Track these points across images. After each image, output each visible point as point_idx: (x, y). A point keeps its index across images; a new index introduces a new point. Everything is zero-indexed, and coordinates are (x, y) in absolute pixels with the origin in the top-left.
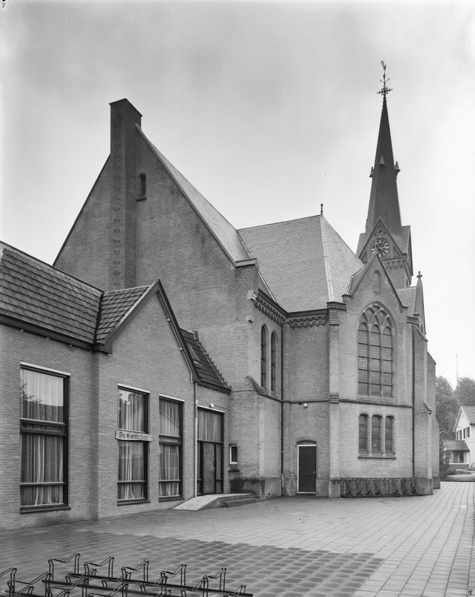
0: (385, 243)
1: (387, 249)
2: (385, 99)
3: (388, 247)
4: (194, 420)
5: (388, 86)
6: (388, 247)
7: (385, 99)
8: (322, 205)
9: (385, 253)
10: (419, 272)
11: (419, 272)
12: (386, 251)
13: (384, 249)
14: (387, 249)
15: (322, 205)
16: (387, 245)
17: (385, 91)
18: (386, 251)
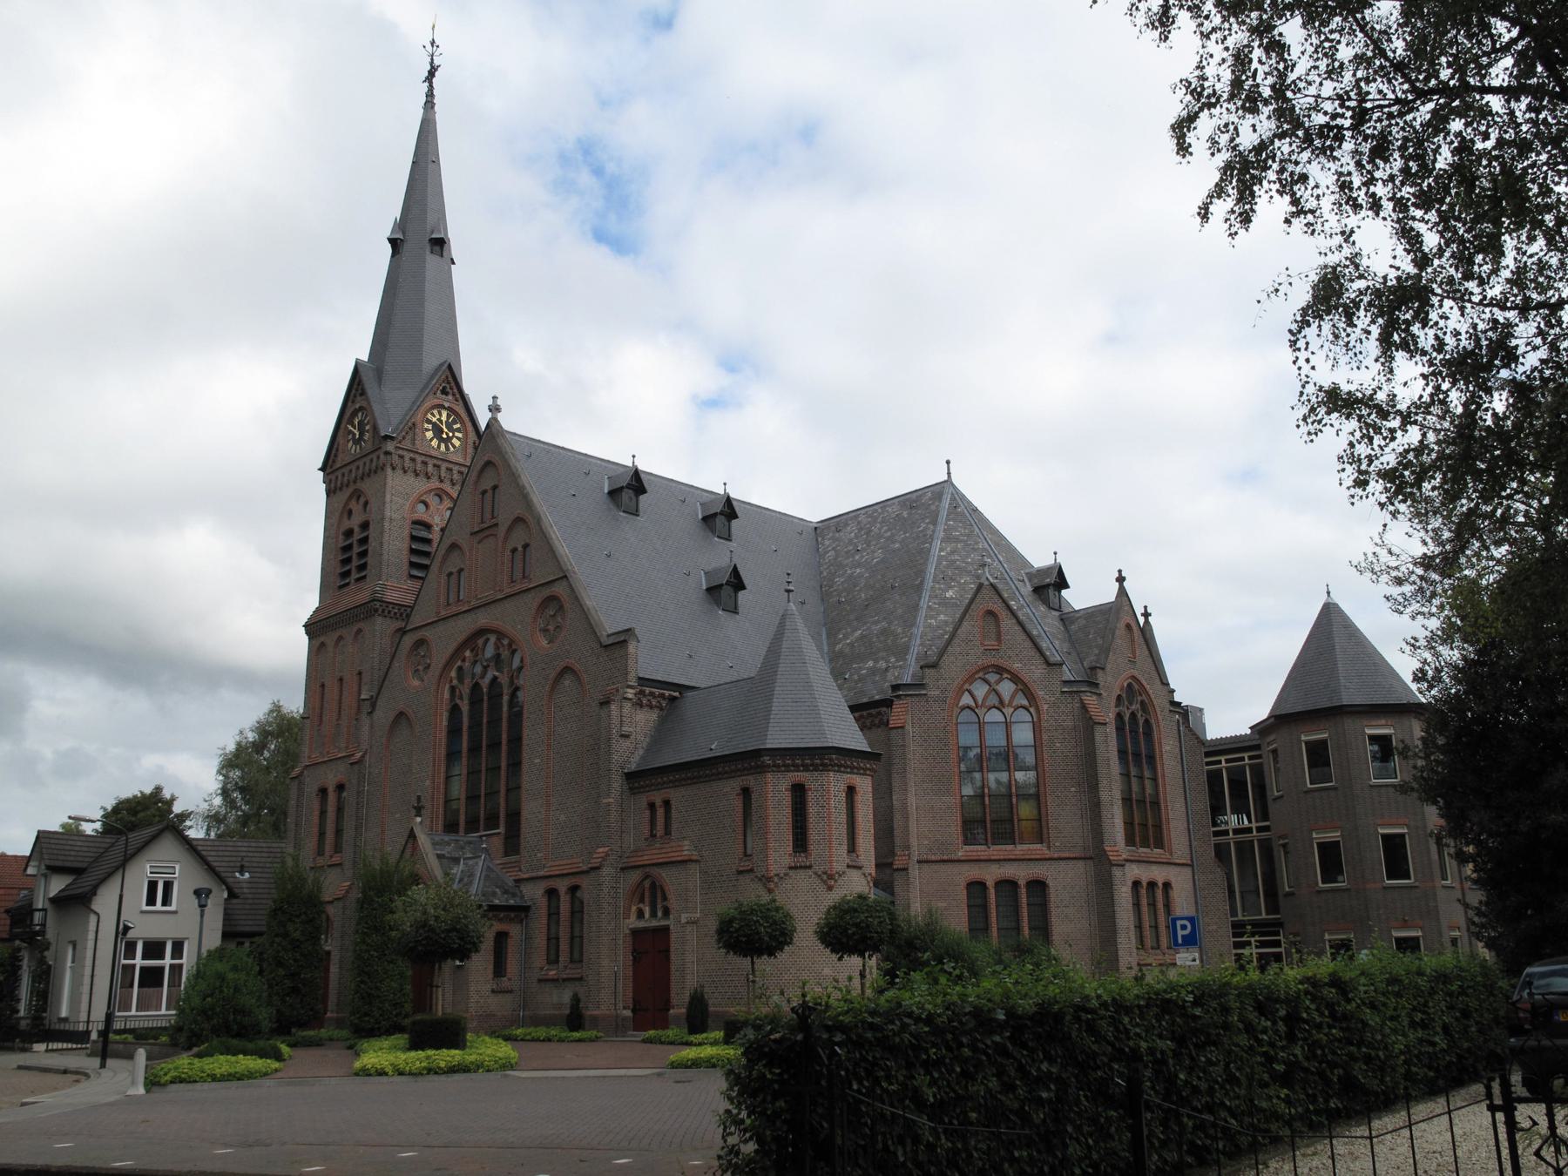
8: (948, 462)
15: (948, 462)
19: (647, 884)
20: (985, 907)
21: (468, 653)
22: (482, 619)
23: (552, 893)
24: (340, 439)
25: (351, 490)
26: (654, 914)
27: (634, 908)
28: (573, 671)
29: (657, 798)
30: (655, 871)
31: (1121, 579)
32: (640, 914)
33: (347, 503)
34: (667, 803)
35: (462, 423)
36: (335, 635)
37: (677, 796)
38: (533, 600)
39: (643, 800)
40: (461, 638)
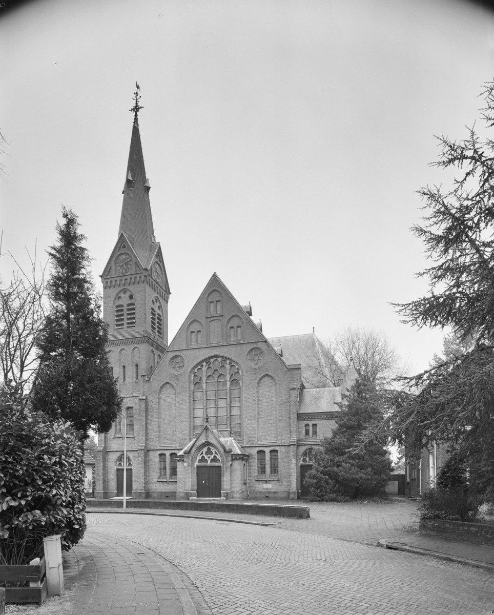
2: (136, 115)
5: (140, 104)
7: (136, 115)
17: (136, 109)
21: (204, 364)
22: (215, 352)
29: (311, 423)
34: (314, 425)
36: (133, 347)
39: (303, 424)
40: (203, 358)
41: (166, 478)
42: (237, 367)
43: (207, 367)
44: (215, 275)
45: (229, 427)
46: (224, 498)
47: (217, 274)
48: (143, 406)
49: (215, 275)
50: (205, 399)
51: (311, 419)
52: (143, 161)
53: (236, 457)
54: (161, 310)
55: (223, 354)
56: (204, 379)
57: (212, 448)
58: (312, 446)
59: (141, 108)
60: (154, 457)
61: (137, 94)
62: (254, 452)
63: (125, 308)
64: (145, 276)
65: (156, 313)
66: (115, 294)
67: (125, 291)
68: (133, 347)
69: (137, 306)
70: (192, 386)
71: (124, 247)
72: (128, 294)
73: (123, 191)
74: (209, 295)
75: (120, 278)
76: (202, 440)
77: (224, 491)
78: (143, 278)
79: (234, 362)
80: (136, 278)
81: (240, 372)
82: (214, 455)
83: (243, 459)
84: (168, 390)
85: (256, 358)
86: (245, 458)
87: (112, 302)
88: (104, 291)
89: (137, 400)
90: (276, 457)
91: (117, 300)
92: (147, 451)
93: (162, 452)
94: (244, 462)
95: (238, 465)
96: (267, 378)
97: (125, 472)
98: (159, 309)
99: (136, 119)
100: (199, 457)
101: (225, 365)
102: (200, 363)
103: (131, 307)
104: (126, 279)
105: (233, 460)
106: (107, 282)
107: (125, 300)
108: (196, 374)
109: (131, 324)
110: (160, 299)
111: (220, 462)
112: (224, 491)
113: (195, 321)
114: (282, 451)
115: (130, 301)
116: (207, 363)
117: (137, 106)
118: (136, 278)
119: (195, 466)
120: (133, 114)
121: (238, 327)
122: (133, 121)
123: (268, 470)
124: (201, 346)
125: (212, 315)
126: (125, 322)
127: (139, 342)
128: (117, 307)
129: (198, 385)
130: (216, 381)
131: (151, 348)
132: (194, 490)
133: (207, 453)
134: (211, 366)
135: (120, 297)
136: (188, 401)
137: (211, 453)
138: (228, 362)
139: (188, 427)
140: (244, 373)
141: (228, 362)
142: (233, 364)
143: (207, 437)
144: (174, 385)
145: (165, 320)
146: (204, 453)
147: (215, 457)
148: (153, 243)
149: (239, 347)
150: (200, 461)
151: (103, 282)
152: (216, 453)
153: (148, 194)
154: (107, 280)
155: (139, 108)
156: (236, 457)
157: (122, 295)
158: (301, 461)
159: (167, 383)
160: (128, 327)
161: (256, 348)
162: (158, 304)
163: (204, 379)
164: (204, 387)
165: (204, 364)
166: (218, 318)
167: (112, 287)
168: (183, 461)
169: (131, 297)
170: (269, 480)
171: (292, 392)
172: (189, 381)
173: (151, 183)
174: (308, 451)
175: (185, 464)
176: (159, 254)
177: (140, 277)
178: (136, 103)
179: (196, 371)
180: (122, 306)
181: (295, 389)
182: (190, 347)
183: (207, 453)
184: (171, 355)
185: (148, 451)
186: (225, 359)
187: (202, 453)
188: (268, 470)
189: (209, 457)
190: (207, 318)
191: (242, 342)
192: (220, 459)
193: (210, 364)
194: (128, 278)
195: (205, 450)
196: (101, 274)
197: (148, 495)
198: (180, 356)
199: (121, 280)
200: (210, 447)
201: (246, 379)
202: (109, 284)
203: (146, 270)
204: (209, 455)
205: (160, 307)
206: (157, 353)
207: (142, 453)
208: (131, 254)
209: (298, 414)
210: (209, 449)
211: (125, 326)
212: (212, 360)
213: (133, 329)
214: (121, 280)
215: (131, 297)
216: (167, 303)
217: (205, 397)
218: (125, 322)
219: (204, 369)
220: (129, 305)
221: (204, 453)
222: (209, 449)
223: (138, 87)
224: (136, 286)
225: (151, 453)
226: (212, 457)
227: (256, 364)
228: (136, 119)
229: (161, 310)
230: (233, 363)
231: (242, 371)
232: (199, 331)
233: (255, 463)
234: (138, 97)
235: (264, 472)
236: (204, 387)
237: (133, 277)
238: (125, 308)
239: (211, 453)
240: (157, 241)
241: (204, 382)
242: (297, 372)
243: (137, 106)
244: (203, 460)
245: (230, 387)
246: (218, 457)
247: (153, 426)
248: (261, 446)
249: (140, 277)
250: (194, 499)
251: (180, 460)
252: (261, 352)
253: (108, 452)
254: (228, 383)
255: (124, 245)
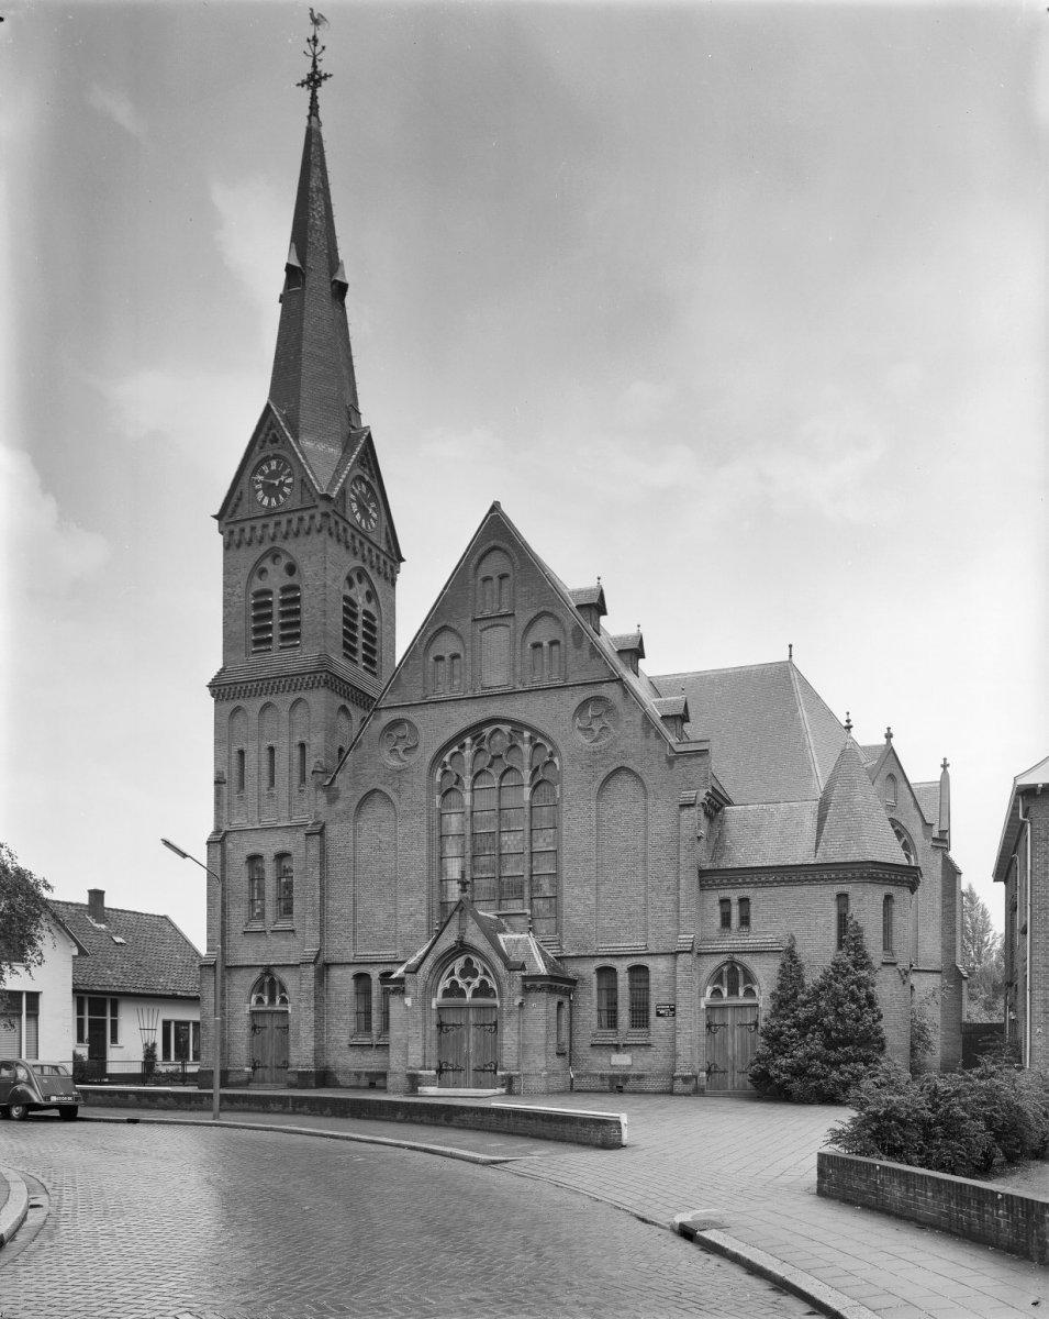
0: (285, 468)
1: (289, 485)
2: (314, 98)
3: (290, 480)
4: (559, 1018)
5: (323, 68)
6: (290, 480)
7: (314, 98)
8: (790, 646)
9: (284, 495)
10: (945, 759)
11: (945, 759)
12: (286, 490)
13: (282, 484)
14: (289, 485)
15: (790, 646)
16: (289, 475)
17: (314, 80)
18: (286, 490)
19: (267, 980)
20: (368, 1013)
21: (468, 741)
22: (495, 709)
23: (606, 973)
24: (244, 485)
25: (264, 548)
26: (272, 1000)
27: (254, 997)
28: (629, 771)
29: (734, 895)
30: (276, 970)
31: (945, 766)
32: (260, 1000)
33: (258, 563)
34: (744, 901)
35: (378, 505)
36: (292, 697)
37: (756, 895)
38: (574, 699)
39: (714, 898)
40: (463, 725)
41: (370, 1036)
42: (549, 749)
43: (475, 748)
44: (495, 507)
45: (527, 903)
46: (504, 1090)
47: (505, 508)
48: (314, 851)
49: (495, 507)
50: (468, 833)
51: (734, 885)
52: (332, 216)
53: (531, 984)
54: (373, 603)
55: (514, 716)
56: (467, 779)
57: (475, 959)
58: (736, 957)
59: (326, 76)
60: (342, 980)
61: (315, 40)
62: (588, 970)
63: (276, 598)
64: (325, 515)
65: (360, 610)
66: (250, 564)
67: (275, 555)
68: (292, 697)
69: (305, 594)
70: (438, 797)
71: (275, 440)
72: (284, 561)
73: (281, 296)
74: (483, 557)
75: (263, 521)
76: (448, 940)
77: (503, 1073)
78: (318, 518)
79: (542, 736)
80: (301, 519)
81: (556, 760)
82: (480, 977)
83: (552, 990)
84: (377, 810)
85: (596, 726)
86: (559, 984)
87: (243, 584)
88: (225, 555)
89: (300, 836)
90: (643, 985)
91: (256, 578)
92: (323, 968)
93: (363, 969)
94: (558, 998)
95: (541, 1008)
96: (624, 777)
97: (191, 1025)
98: (369, 601)
99: (314, 108)
100: (445, 984)
101: (519, 743)
102: (457, 739)
103: (290, 596)
104: (278, 524)
105: (526, 990)
106: (232, 533)
107: (276, 579)
108: (449, 768)
109: (292, 635)
110: (372, 575)
111: (495, 996)
112: (503, 1073)
113: (444, 628)
114: (658, 967)
115: (289, 581)
116: (474, 739)
117: (315, 72)
118: (301, 519)
119: (434, 1006)
120: (306, 93)
121: (552, 643)
122: (308, 112)
123: (624, 1017)
124: (460, 695)
125: (487, 613)
126: (275, 634)
127: (284, 687)
128: (257, 594)
129: (453, 797)
130: (496, 785)
131: (342, 702)
132: (430, 1069)
133: (463, 974)
134: (485, 746)
135: (263, 571)
136: (424, 836)
137: (475, 974)
138: (527, 734)
139: (425, 906)
140: (566, 762)
141: (527, 734)
142: (539, 740)
143: (462, 930)
144: (394, 797)
145: (386, 628)
146: (457, 971)
147: (483, 982)
148: (353, 427)
149: (554, 697)
150: (447, 993)
151: (221, 533)
152: (486, 973)
153: (343, 305)
154: (232, 527)
155: (321, 78)
156: (531, 984)
157: (267, 564)
158: (440, 994)
159: (375, 791)
160: (281, 648)
161: (598, 699)
162: (365, 587)
163: (467, 779)
164: (468, 801)
165: (468, 741)
166: (501, 621)
167: (244, 546)
168: (403, 992)
169: (291, 569)
170: (625, 1045)
171: (686, 813)
172: (430, 789)
173: (349, 274)
174: (725, 969)
175: (408, 1001)
176: (369, 457)
177: (312, 517)
178: (314, 66)
179: (446, 759)
180: (269, 593)
181: (692, 805)
182: (434, 697)
183: (463, 974)
184: (386, 717)
185: (328, 966)
186: (518, 726)
187: (452, 973)
188: (624, 1017)
189: (469, 984)
190: (475, 620)
191: (559, 683)
192: (495, 988)
193: (483, 740)
194: (284, 519)
195: (459, 964)
196: (216, 512)
197: (324, 1077)
198: (408, 722)
199: (265, 526)
200: (470, 956)
201: (574, 786)
202: (236, 537)
203: (326, 498)
204: (468, 979)
205: (370, 596)
206: (357, 713)
207: (311, 971)
208: (292, 460)
209: (700, 871)
210: (469, 962)
211: (277, 643)
212: (487, 731)
213: (267, 655)
214: (265, 526)
215: (291, 569)
216: (394, 585)
217: (468, 824)
218: (275, 634)
219: (468, 753)
220: (284, 590)
221: (457, 971)
222: (469, 962)
223: (316, 22)
224: (302, 539)
225: (336, 973)
226: (476, 983)
227: (596, 741)
228: (314, 108)
229: (373, 603)
230: (538, 740)
231: (561, 760)
232: (455, 657)
233: (589, 1003)
234: (318, 49)
235: (613, 1023)
236: (468, 801)
237: (295, 517)
238: (276, 598)
239: (475, 974)
240: (364, 424)
241: (468, 787)
242: (699, 760)
243: (315, 72)
244: (454, 991)
245: (531, 802)
246: (492, 984)
247: (339, 904)
248: (607, 956)
249: (312, 517)
250: (432, 1092)
251: (395, 991)
252: (610, 709)
253: (231, 967)
254: (527, 791)
255: (274, 435)
